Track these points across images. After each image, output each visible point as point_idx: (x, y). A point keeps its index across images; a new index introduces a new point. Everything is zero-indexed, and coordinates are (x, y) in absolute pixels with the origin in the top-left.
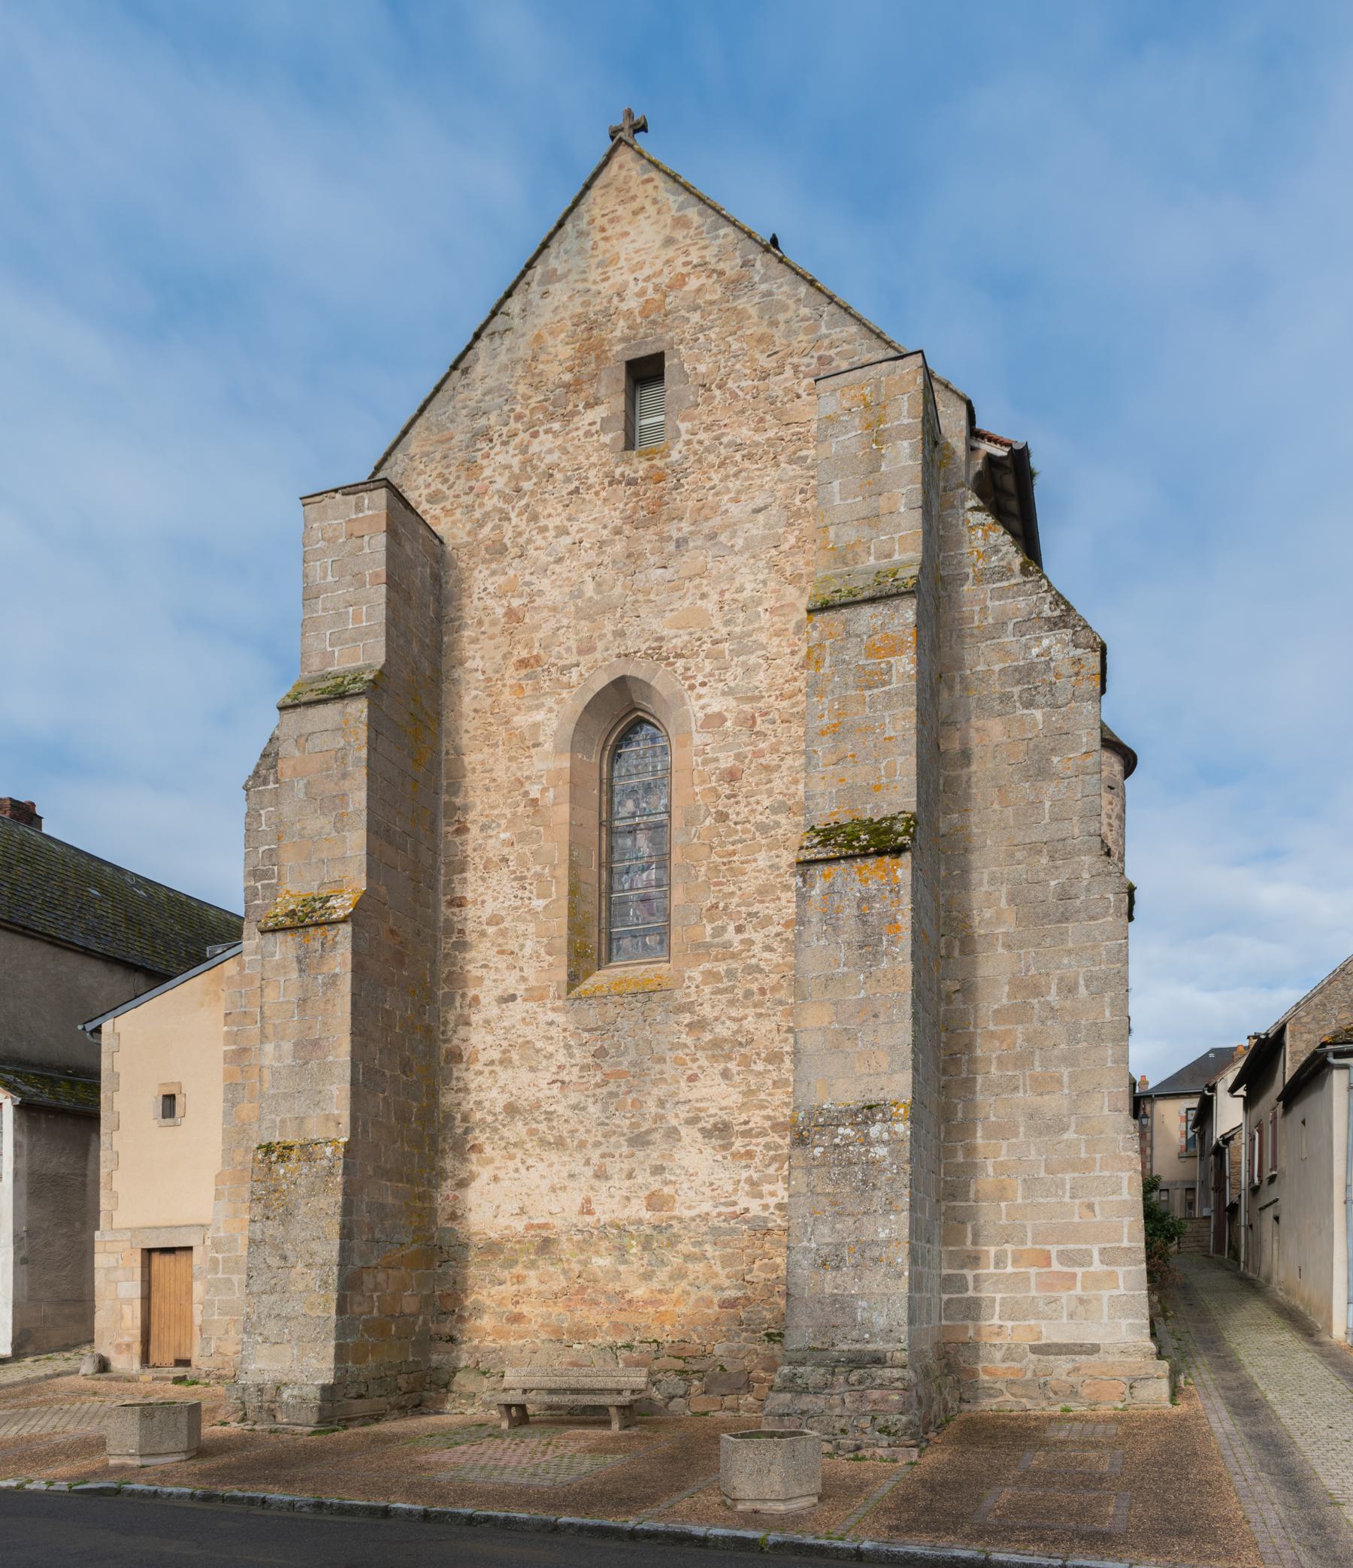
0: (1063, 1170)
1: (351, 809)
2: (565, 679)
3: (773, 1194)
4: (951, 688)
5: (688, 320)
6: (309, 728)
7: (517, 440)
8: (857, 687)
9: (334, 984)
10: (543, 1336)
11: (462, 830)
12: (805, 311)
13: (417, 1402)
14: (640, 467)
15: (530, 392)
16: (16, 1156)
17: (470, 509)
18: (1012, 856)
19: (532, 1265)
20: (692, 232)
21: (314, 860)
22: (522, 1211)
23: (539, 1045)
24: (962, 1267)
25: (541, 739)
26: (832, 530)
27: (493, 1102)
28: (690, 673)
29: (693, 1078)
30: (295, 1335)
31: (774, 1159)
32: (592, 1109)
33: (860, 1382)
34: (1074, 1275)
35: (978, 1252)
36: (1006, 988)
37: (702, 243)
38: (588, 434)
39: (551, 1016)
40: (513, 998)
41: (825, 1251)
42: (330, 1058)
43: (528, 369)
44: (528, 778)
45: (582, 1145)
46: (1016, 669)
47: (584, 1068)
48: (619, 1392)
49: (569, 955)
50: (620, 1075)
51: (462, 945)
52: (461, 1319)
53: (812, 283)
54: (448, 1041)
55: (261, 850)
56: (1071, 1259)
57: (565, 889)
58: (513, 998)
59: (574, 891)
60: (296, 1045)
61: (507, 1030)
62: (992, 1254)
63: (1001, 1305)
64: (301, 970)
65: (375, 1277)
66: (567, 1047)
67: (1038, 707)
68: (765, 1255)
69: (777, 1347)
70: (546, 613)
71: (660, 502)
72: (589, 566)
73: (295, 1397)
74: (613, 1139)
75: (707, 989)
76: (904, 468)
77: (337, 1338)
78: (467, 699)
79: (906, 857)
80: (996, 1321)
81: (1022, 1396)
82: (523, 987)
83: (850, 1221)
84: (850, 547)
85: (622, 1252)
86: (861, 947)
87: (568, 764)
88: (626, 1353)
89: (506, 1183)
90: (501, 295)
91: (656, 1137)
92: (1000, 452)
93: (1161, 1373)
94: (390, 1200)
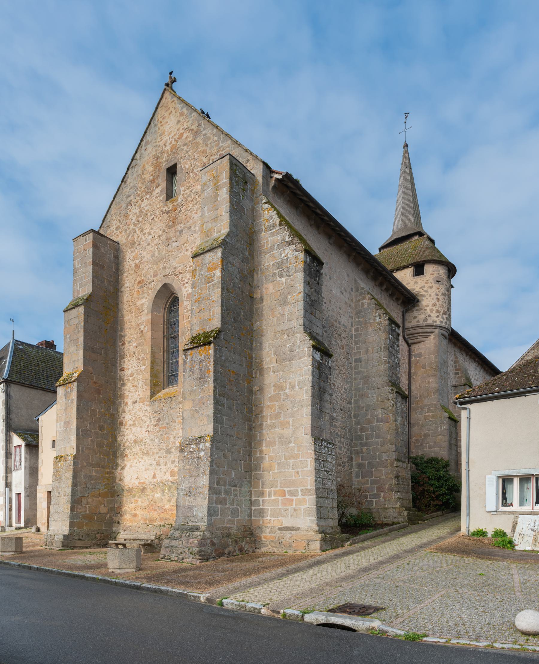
0: (290, 459)
2: (150, 287)
4: (257, 273)
5: (183, 149)
7: (138, 203)
8: (204, 284)
10: (142, 522)
11: (124, 344)
12: (216, 138)
13: (105, 543)
14: (170, 206)
15: (141, 186)
16: (25, 462)
17: (126, 230)
18: (275, 336)
19: (140, 497)
20: (184, 117)
22: (138, 478)
24: (258, 497)
26: (205, 225)
27: (131, 439)
28: (183, 279)
32: (156, 441)
33: (189, 536)
34: (293, 500)
35: (263, 491)
36: (273, 388)
37: (187, 120)
38: (157, 197)
39: (146, 408)
40: (136, 402)
41: (186, 490)
43: (141, 177)
44: (140, 323)
45: (153, 453)
46: (278, 263)
48: (147, 540)
49: (151, 386)
50: (163, 428)
51: (123, 384)
52: (121, 516)
53: (217, 127)
54: (119, 418)
56: (292, 493)
57: (150, 362)
58: (136, 402)
59: (153, 362)
61: (135, 413)
62: (268, 492)
63: (270, 511)
64: (66, 398)
65: (87, 500)
66: (150, 418)
67: (284, 277)
70: (145, 264)
71: (175, 218)
72: (156, 245)
74: (161, 451)
76: (224, 198)
77: (70, 520)
78: (125, 298)
79: (212, 345)
80: (269, 518)
81: (274, 547)
82: (139, 398)
83: (193, 478)
84: (209, 230)
86: (200, 379)
87: (150, 317)
89: (133, 468)
90: (134, 153)
92: (280, 177)
93: (318, 539)
94: (94, 474)
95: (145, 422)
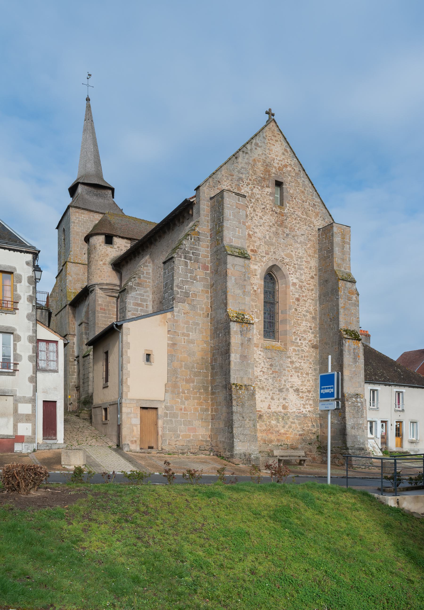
1: (246, 290)
3: (308, 408)
6: (235, 263)
9: (250, 341)
21: (237, 302)
23: (257, 360)
25: (257, 274)
29: (291, 376)
30: (248, 440)
31: (307, 399)
39: (260, 352)
42: (249, 362)
44: (254, 283)
45: (268, 390)
47: (268, 369)
50: (276, 372)
53: (312, 185)
55: (180, 279)
60: (240, 356)
64: (241, 335)
68: (307, 423)
69: (311, 446)
73: (255, 457)
74: (275, 389)
75: (294, 353)
83: (356, 419)
85: (278, 419)
88: (281, 447)
91: (284, 390)
95: (260, 364)
